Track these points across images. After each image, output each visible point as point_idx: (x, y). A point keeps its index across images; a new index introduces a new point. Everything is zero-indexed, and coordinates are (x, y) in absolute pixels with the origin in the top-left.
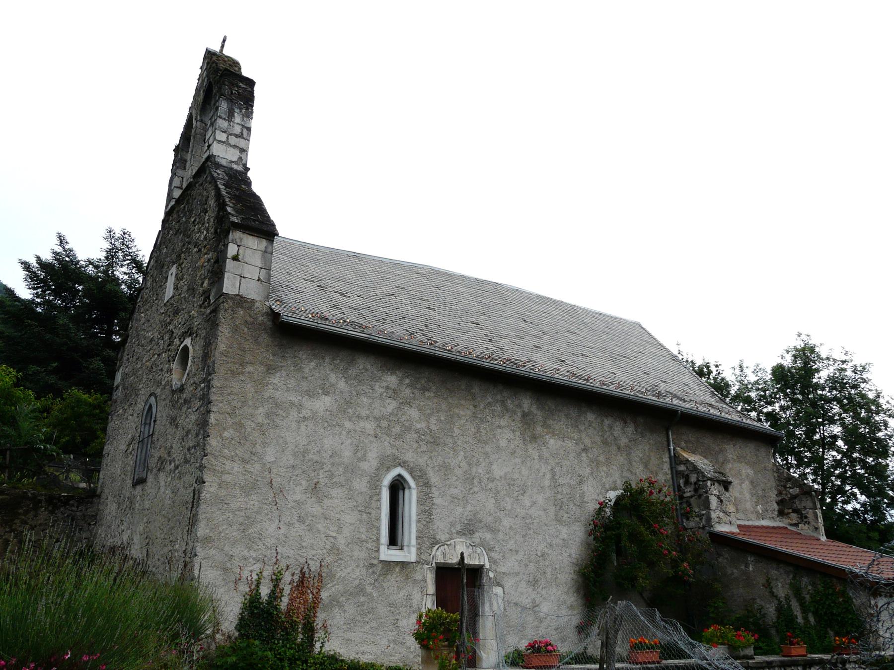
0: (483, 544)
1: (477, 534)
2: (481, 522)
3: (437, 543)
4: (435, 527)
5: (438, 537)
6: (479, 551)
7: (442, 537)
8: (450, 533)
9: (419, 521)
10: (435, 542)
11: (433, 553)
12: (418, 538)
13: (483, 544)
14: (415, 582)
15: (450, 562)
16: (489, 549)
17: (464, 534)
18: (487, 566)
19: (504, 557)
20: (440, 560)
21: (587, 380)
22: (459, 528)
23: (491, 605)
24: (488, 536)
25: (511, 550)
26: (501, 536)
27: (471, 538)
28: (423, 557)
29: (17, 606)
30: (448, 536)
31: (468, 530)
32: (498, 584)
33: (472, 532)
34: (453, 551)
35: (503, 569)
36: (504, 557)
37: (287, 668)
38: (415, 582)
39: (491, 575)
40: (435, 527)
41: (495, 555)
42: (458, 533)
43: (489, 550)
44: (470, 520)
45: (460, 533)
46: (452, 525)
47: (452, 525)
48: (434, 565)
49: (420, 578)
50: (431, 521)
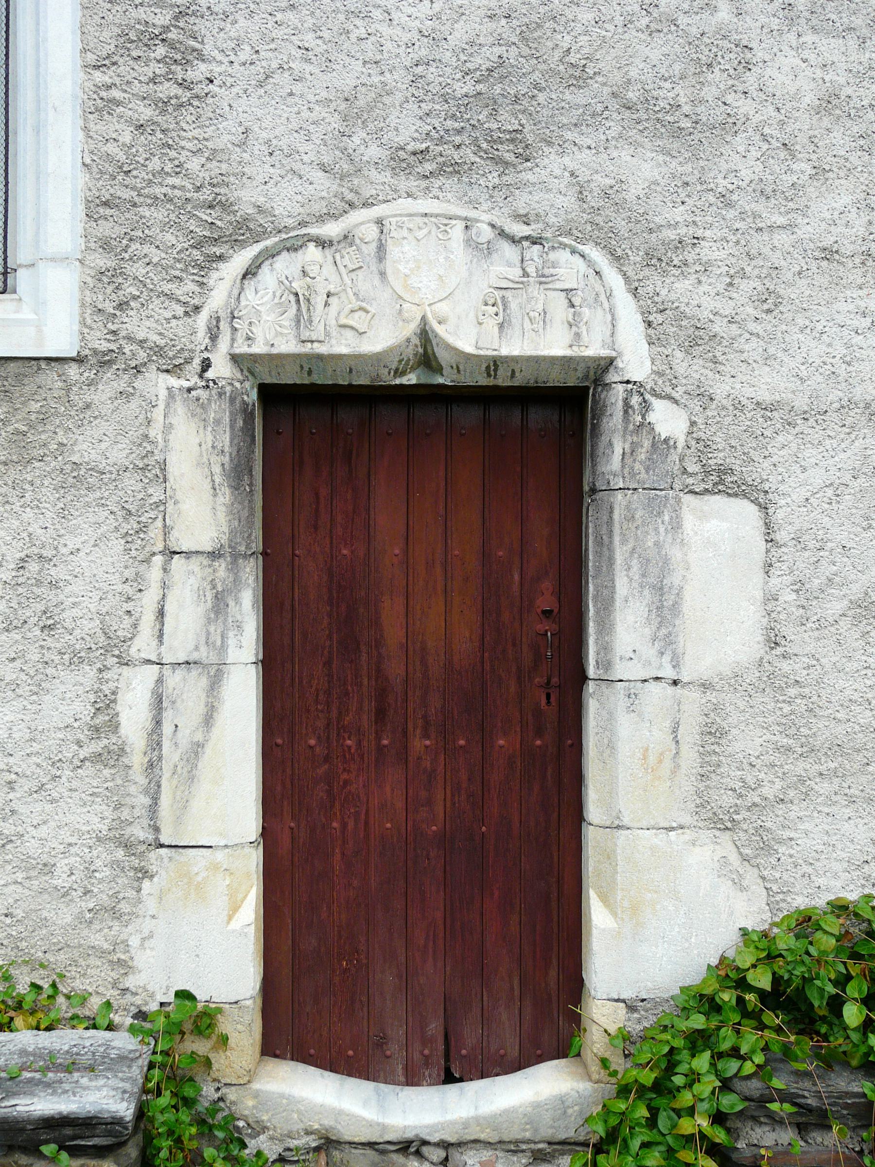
0: (603, 224)
1: (552, 164)
2: (578, 76)
3: (243, 232)
4: (224, 135)
5: (247, 197)
6: (569, 268)
7: (277, 194)
8: (345, 169)
9: (101, 105)
10: (223, 231)
11: (217, 299)
12: (98, 207)
13: (603, 224)
14: (78, 477)
15: (342, 345)
16: (651, 257)
17: (454, 169)
18: (636, 362)
19: (769, 302)
20: (272, 334)
21: (855, 964)
22: (406, 127)
23: (665, 609)
24: (641, 168)
25: (829, 254)
26: (741, 162)
27: (507, 190)
28: (135, 324)
29: (116, 864)
30: (324, 185)
31: (479, 134)
32: (721, 482)
33: (509, 152)
34: (366, 282)
35: (767, 384)
36: (769, 302)
37: (3, 952)
38: (78, 477)
39: (668, 420)
40: (224, 135)
41: (695, 295)
42: (407, 161)
43: (654, 259)
44: (497, 70)
45: (418, 163)
46: (355, 111)
47: (355, 111)
48: (222, 369)
49: (119, 455)
50: (195, 95)
